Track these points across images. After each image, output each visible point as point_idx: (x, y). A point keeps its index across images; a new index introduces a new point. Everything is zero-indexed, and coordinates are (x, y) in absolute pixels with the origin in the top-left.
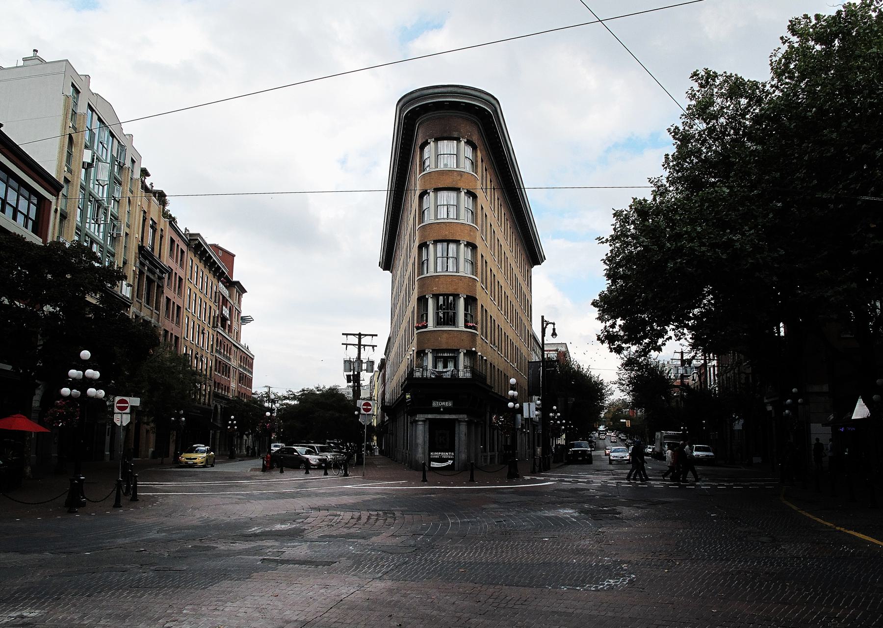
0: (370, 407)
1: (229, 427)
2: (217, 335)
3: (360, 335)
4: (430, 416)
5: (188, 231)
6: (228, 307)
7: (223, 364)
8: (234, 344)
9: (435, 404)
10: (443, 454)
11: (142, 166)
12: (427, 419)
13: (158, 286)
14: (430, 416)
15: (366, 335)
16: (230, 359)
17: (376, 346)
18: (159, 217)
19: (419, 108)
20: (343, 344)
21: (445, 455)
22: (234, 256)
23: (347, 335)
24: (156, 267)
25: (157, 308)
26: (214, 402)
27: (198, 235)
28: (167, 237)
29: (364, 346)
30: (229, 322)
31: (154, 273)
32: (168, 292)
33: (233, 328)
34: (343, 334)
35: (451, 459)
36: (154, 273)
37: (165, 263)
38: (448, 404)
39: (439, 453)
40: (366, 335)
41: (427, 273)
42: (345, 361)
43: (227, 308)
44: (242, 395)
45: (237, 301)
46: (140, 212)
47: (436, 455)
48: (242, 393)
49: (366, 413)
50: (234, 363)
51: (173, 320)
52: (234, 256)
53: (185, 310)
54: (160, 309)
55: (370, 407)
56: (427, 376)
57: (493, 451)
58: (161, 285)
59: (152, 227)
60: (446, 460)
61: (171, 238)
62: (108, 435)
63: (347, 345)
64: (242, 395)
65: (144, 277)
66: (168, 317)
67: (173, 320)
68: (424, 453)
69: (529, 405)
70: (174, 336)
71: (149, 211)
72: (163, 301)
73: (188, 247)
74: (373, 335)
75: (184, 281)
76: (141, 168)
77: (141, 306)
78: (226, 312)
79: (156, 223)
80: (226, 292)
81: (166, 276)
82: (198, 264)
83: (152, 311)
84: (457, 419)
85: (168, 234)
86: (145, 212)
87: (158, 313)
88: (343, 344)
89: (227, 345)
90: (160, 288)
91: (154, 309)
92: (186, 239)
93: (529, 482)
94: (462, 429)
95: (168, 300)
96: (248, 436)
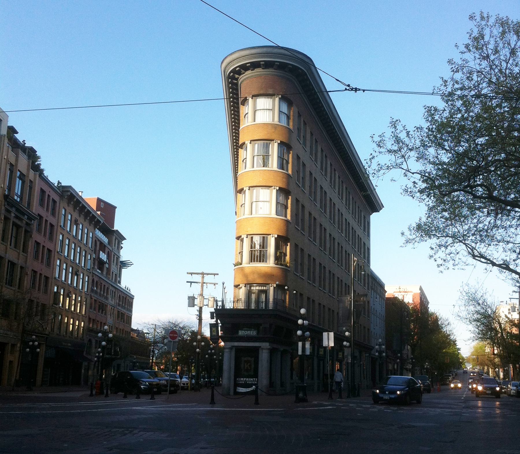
0: (177, 335)
1: (28, 350)
2: (93, 276)
3: (203, 274)
4: (236, 344)
5: (61, 183)
6: (106, 252)
7: (99, 302)
8: (111, 285)
9: (241, 333)
10: (247, 379)
11: (8, 125)
12: (233, 346)
13: (26, 231)
14: (236, 344)
15: (208, 274)
16: (107, 298)
17: (217, 284)
18: (28, 170)
19: (249, 65)
20: (187, 282)
21: (250, 380)
22: (116, 208)
23: (192, 274)
24: (23, 214)
25: (25, 250)
26: (88, 336)
27: (70, 187)
28: (36, 188)
29: (207, 283)
30: (107, 266)
31: (21, 220)
32: (36, 237)
33: (112, 271)
34: (187, 273)
35: (254, 385)
36: (21, 220)
37: (34, 211)
38: (253, 333)
39: (245, 379)
40: (208, 274)
41: (256, 213)
42: (189, 297)
43: (104, 253)
44: (120, 331)
45: (116, 247)
46: (6, 164)
47: (242, 380)
48: (126, 331)
49: (172, 340)
50: (111, 302)
51: (42, 262)
52: (116, 208)
53: (56, 253)
54: (27, 252)
55: (177, 335)
56: (233, 307)
57: (313, 379)
58: (29, 230)
59: (20, 178)
60: (250, 386)
61: (41, 189)
62: (11, 362)
63: (191, 282)
64: (120, 331)
65: (10, 223)
66: (38, 259)
67: (42, 262)
68: (229, 378)
69: (328, 334)
70: (43, 276)
71: (16, 164)
72: (31, 245)
73: (60, 197)
74: (214, 275)
75: (55, 227)
76: (8, 126)
77: (6, 249)
78: (103, 256)
79: (24, 175)
80: (105, 240)
81: (35, 223)
82: (72, 213)
83: (19, 253)
84: (260, 347)
85: (38, 185)
86: (11, 165)
87: (26, 255)
88: (187, 282)
89: (104, 285)
90: (28, 233)
91: (21, 251)
92: (59, 191)
93: (316, 406)
94: (264, 356)
95: (38, 244)
96: (394, 392)
